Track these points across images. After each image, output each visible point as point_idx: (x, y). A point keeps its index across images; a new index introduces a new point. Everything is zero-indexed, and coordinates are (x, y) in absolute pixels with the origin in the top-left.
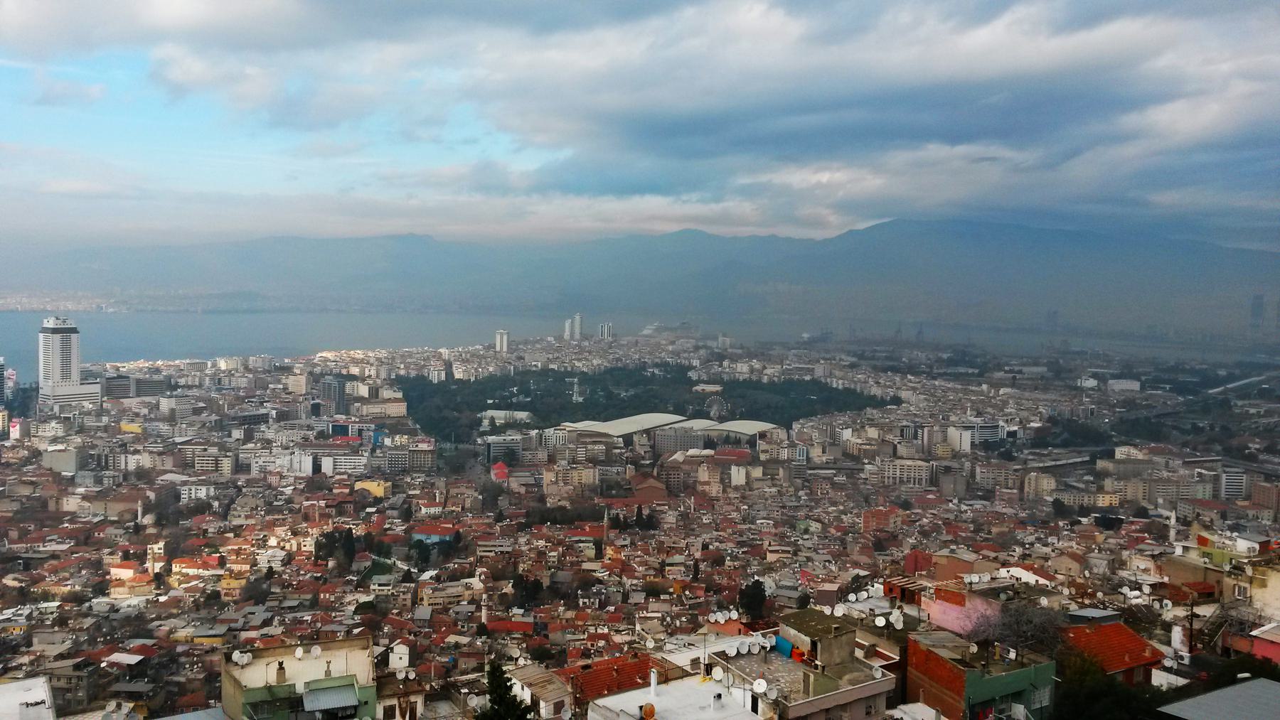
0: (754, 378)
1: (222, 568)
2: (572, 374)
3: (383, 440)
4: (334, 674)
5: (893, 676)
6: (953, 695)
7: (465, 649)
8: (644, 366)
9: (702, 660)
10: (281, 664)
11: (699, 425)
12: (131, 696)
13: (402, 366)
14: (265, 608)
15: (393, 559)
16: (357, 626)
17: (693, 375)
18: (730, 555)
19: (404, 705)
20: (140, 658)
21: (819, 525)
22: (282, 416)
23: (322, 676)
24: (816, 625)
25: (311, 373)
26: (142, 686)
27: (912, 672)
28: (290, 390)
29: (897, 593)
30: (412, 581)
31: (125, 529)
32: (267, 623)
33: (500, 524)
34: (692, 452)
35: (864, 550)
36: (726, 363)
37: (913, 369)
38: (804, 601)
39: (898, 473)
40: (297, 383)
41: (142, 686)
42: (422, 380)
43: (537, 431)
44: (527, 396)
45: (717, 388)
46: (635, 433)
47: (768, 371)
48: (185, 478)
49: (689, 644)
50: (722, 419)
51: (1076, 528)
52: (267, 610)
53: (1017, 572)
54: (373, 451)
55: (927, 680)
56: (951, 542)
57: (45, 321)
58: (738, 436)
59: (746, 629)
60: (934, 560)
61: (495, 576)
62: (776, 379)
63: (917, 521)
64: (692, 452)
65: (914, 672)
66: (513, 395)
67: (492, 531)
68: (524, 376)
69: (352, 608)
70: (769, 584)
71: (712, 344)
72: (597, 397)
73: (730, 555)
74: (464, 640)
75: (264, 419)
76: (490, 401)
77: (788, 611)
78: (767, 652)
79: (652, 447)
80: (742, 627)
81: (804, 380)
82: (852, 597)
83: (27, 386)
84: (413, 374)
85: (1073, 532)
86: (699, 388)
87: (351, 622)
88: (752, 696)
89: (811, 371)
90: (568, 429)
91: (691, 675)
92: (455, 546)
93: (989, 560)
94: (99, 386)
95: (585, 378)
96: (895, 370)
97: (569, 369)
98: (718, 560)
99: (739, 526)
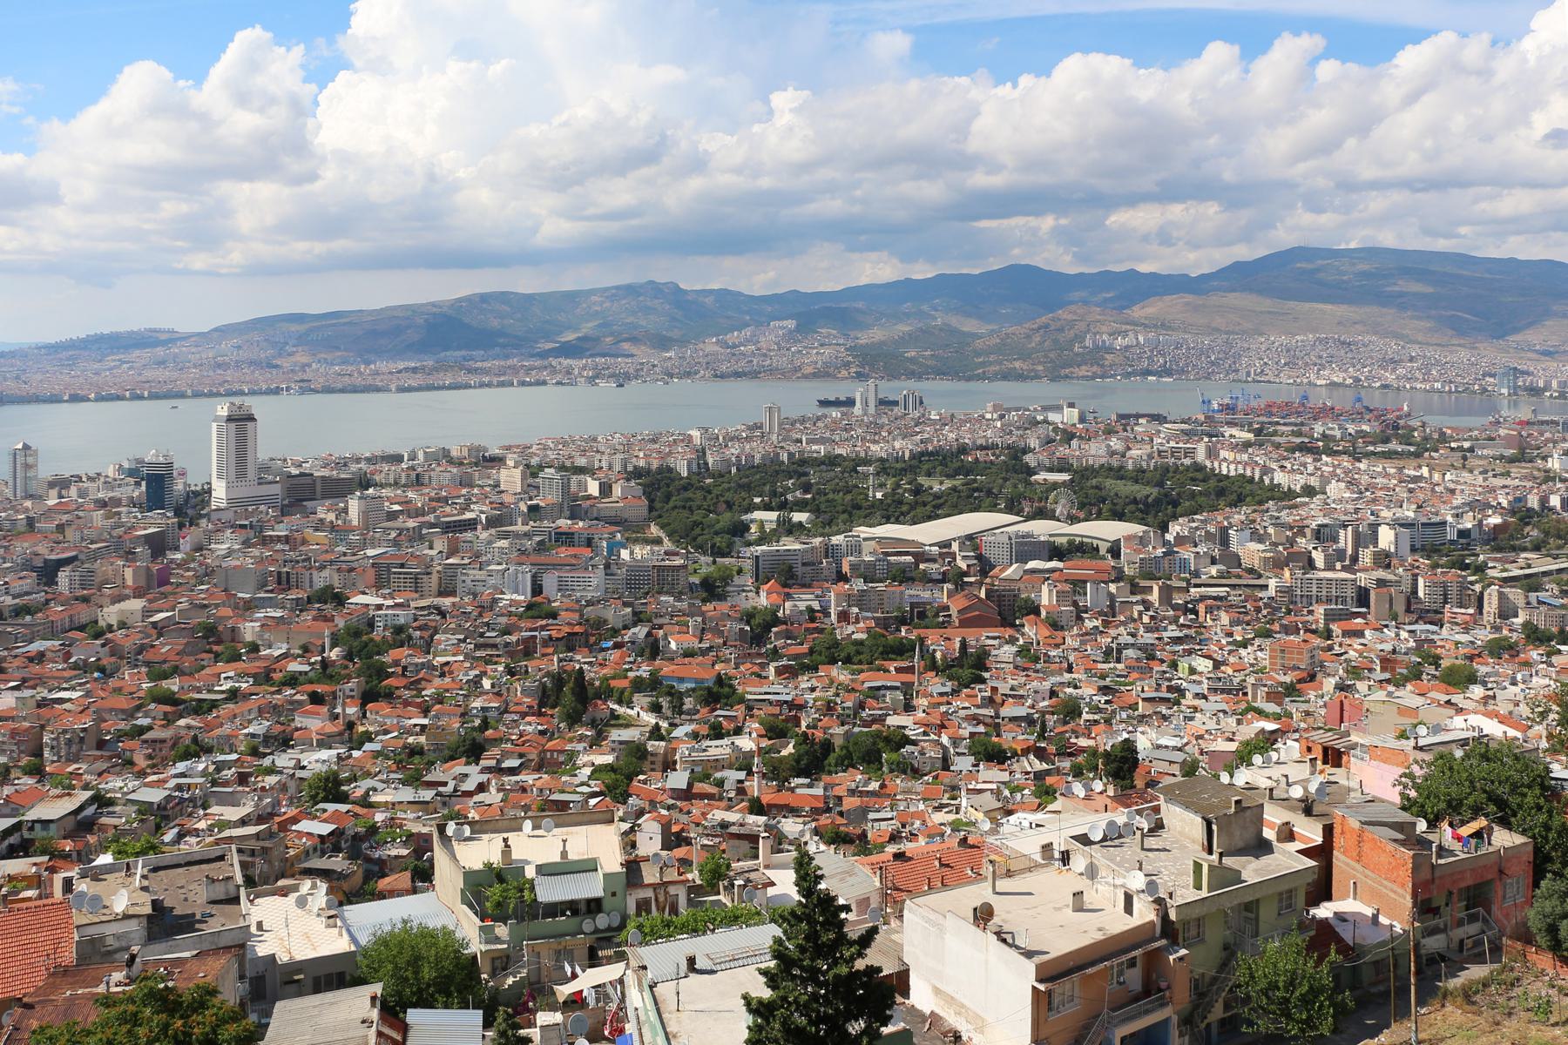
0: (1115, 463)
1: (425, 717)
2: (866, 462)
3: (619, 552)
4: (572, 856)
5: (1314, 863)
6: (1395, 887)
7: (733, 829)
8: (963, 450)
9: (1055, 846)
10: (505, 840)
11: (1041, 529)
12: (325, 874)
13: (641, 455)
14: (479, 768)
15: (637, 709)
16: (594, 795)
17: (1029, 459)
18: (1088, 704)
19: (661, 899)
20: (333, 827)
21: (1210, 663)
22: (492, 522)
23: (557, 859)
24: (1210, 797)
25: (528, 466)
26: (338, 863)
27: (1339, 859)
28: (502, 488)
29: (1318, 753)
30: (661, 738)
31: (310, 664)
32: (482, 788)
33: (776, 664)
34: (1032, 565)
35: (1272, 696)
36: (1075, 443)
37: (1328, 447)
38: (1190, 769)
39: (1314, 589)
40: (511, 478)
41: (338, 863)
42: (667, 473)
43: (820, 539)
44: (806, 491)
45: (1065, 477)
46: (954, 540)
47: (1134, 453)
48: (379, 601)
49: (1037, 825)
50: (1073, 520)
51: (1555, 659)
52: (482, 772)
53: (1477, 720)
54: (542, 733)
55: (1361, 869)
56: (1388, 681)
57: (219, 407)
58: (1095, 542)
59: (1115, 804)
60: (1366, 706)
61: (776, 731)
62: (1144, 464)
63: (1341, 654)
64: (1032, 565)
65: (1343, 858)
66: (787, 490)
67: (764, 674)
68: (800, 465)
69: (587, 771)
70: (1143, 743)
71: (1053, 417)
72: (900, 491)
73: (1088, 704)
74: (732, 817)
75: (471, 525)
76: (757, 500)
77: (1171, 780)
78: (1143, 835)
79: (980, 557)
80: (1108, 801)
81: (1182, 464)
82: (1257, 759)
83: (199, 488)
84: (655, 465)
85: (1551, 665)
86: (1041, 477)
87: (585, 789)
88: (1126, 894)
89: (1189, 453)
90: (862, 536)
91: (1042, 866)
92: (718, 694)
93: (1440, 705)
94: (279, 485)
95: (885, 467)
96: (1303, 448)
97: (863, 455)
98: (1071, 711)
99: (1100, 666)
